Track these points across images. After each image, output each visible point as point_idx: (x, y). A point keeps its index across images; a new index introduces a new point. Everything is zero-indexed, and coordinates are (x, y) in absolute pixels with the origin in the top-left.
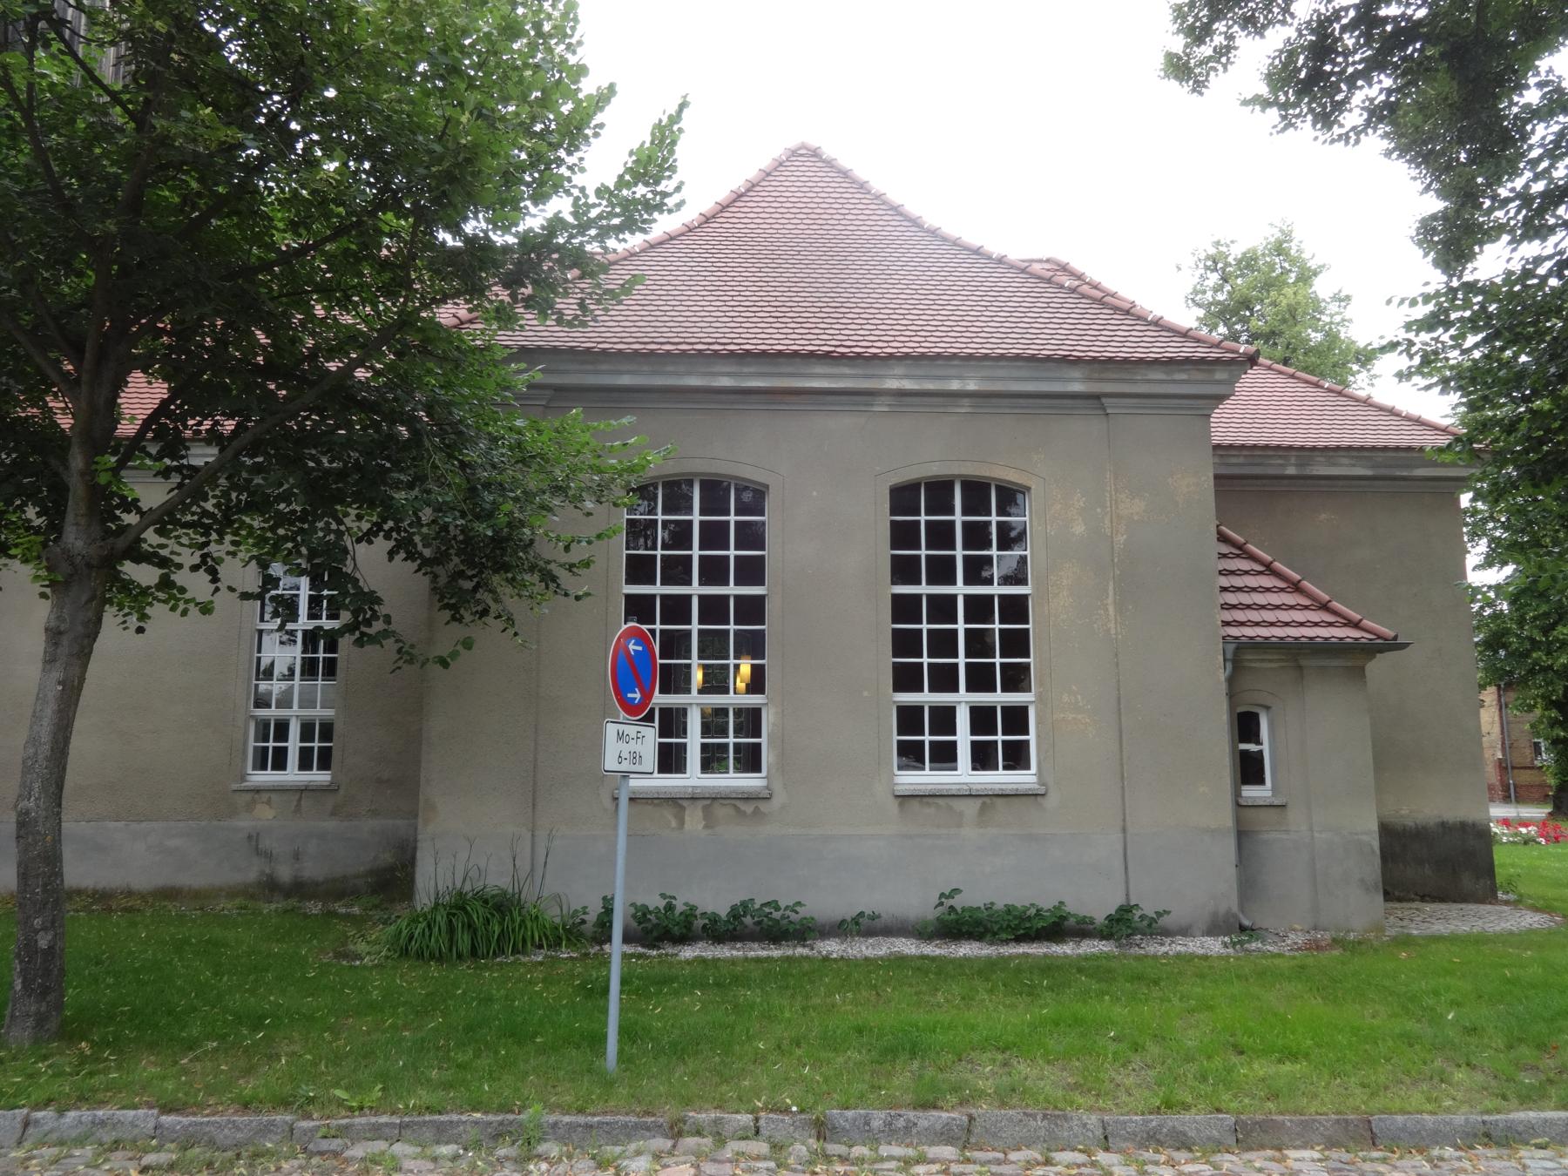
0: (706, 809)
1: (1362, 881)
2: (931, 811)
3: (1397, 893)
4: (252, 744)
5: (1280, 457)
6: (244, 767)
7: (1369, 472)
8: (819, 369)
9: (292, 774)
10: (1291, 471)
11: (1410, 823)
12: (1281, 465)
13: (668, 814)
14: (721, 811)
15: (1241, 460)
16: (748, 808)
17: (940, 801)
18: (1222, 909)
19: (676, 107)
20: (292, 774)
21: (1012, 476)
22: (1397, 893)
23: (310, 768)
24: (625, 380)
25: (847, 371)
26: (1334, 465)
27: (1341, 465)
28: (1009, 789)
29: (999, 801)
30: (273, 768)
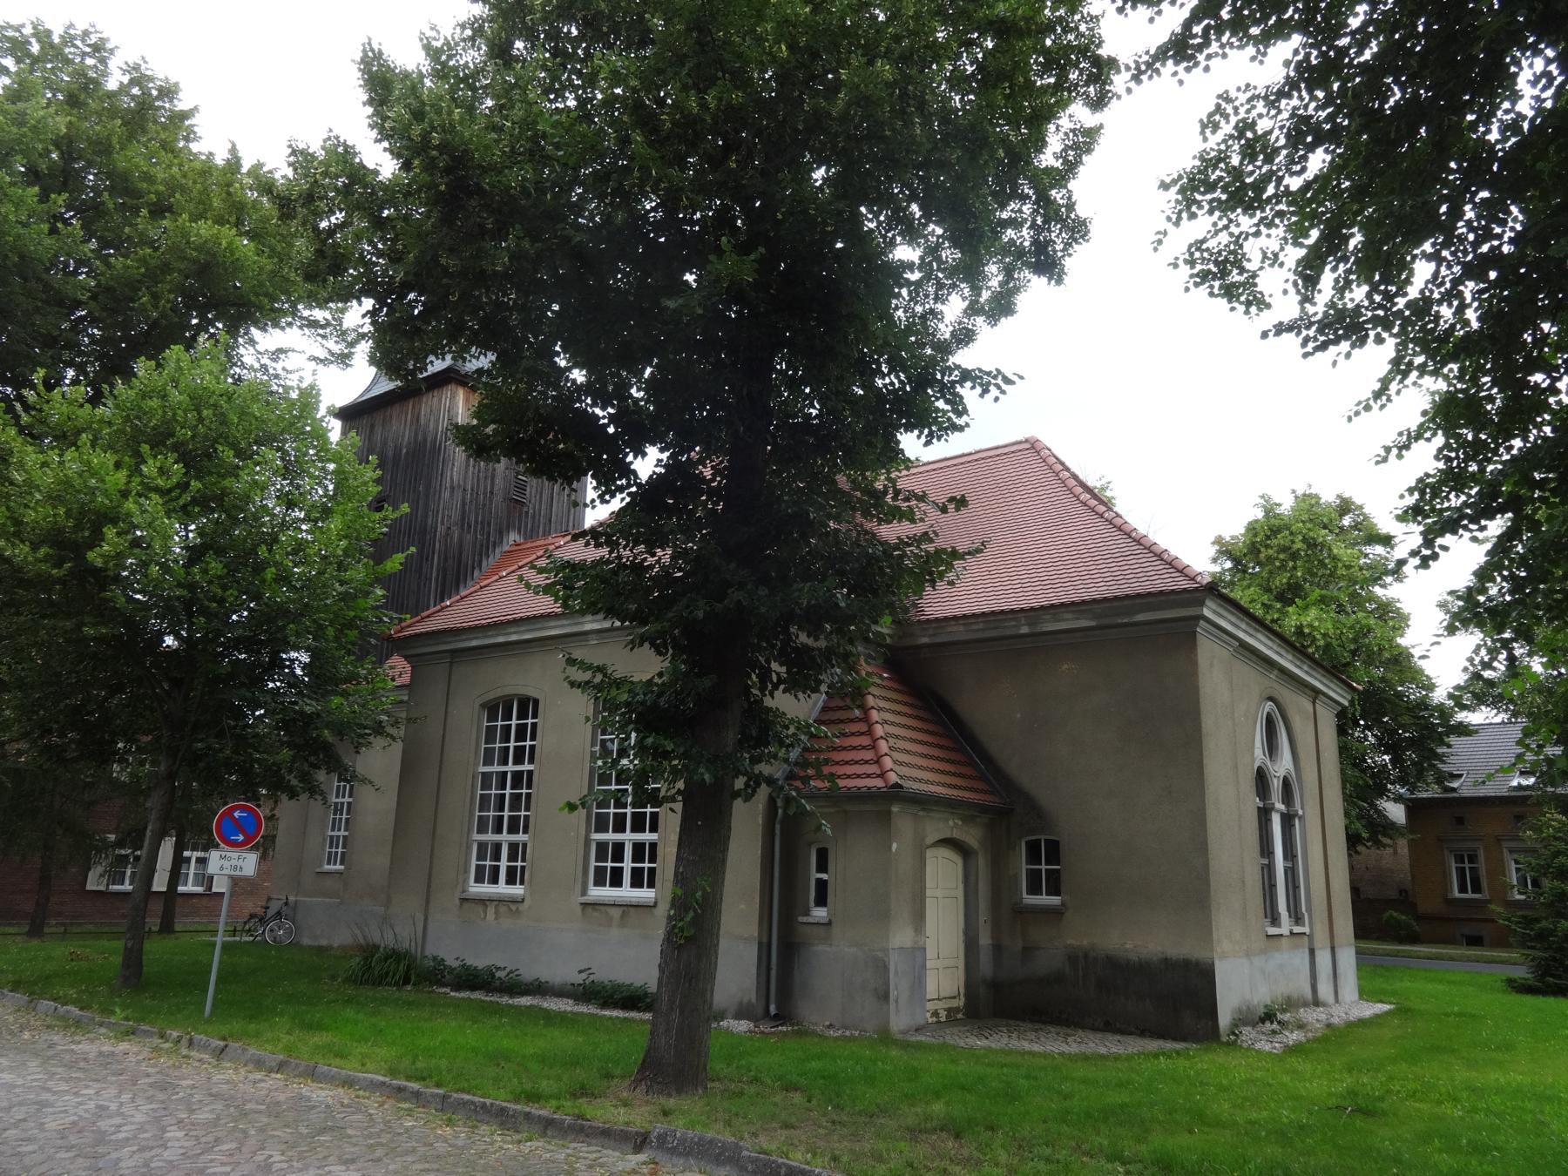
0: (496, 906)
1: (876, 989)
2: (596, 914)
3: (1118, 1025)
4: (474, 862)
5: (1012, 619)
6: (466, 881)
7: (1093, 623)
8: (552, 624)
9: (626, 892)
10: (1025, 630)
11: (1133, 957)
12: (1015, 626)
13: (480, 909)
14: (503, 909)
15: (981, 626)
16: (513, 907)
17: (602, 908)
18: (745, 1000)
19: (1022, 300)
20: (626, 892)
21: (532, 692)
22: (1118, 1025)
23: (604, 885)
24: (474, 643)
25: (565, 622)
26: (1059, 621)
27: (1063, 620)
28: (634, 902)
29: (632, 909)
30: (611, 885)
